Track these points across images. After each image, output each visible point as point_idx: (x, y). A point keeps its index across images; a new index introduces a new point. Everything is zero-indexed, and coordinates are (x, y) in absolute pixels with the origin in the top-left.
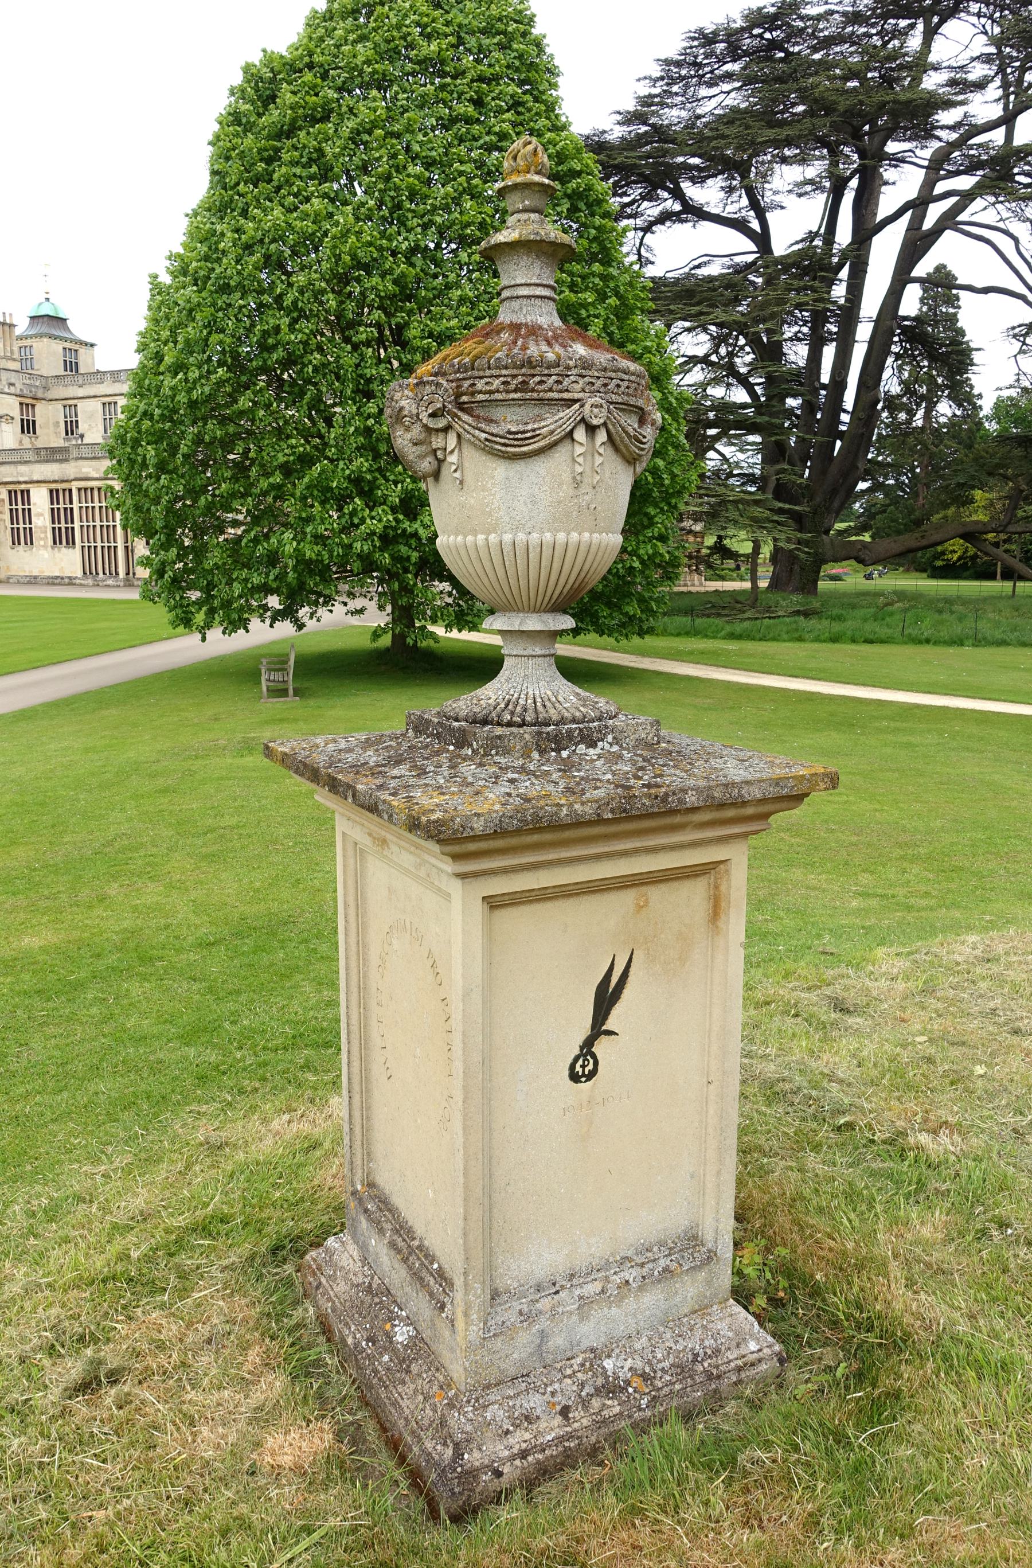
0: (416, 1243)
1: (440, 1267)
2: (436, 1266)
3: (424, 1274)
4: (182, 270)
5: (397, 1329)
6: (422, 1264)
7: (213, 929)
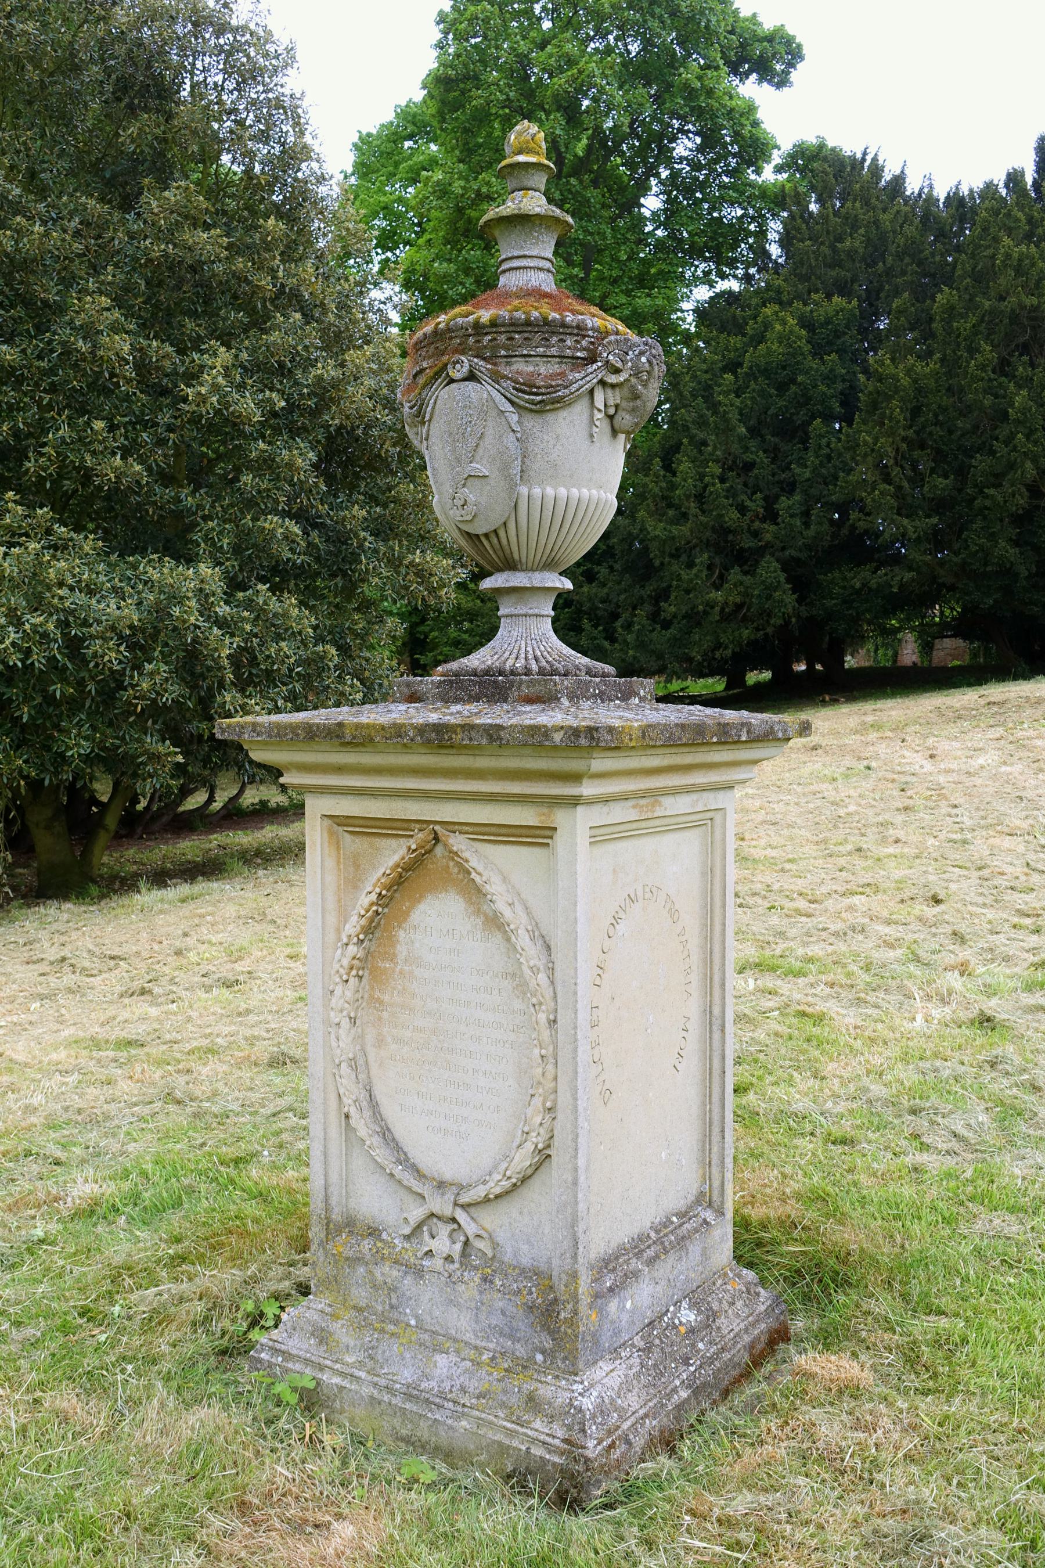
0: (653, 1235)
1: (676, 1215)
2: (674, 1219)
3: (681, 1232)
4: (955, 200)
5: (684, 1321)
6: (672, 1232)
7: (103, 1415)
